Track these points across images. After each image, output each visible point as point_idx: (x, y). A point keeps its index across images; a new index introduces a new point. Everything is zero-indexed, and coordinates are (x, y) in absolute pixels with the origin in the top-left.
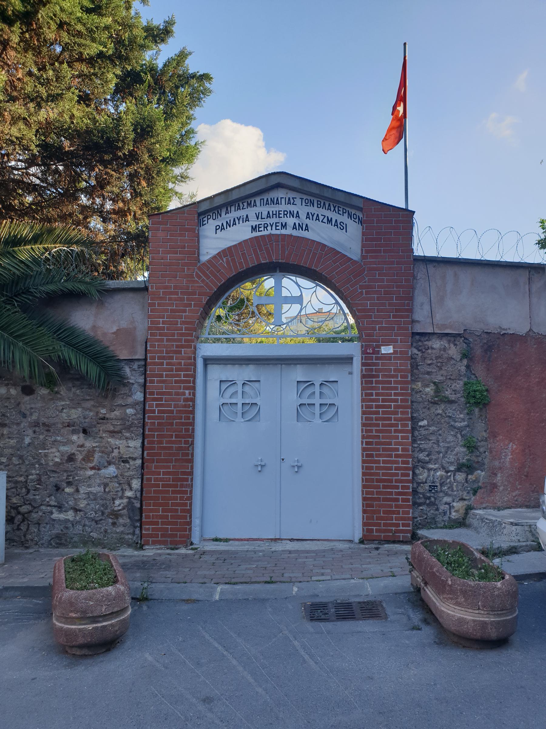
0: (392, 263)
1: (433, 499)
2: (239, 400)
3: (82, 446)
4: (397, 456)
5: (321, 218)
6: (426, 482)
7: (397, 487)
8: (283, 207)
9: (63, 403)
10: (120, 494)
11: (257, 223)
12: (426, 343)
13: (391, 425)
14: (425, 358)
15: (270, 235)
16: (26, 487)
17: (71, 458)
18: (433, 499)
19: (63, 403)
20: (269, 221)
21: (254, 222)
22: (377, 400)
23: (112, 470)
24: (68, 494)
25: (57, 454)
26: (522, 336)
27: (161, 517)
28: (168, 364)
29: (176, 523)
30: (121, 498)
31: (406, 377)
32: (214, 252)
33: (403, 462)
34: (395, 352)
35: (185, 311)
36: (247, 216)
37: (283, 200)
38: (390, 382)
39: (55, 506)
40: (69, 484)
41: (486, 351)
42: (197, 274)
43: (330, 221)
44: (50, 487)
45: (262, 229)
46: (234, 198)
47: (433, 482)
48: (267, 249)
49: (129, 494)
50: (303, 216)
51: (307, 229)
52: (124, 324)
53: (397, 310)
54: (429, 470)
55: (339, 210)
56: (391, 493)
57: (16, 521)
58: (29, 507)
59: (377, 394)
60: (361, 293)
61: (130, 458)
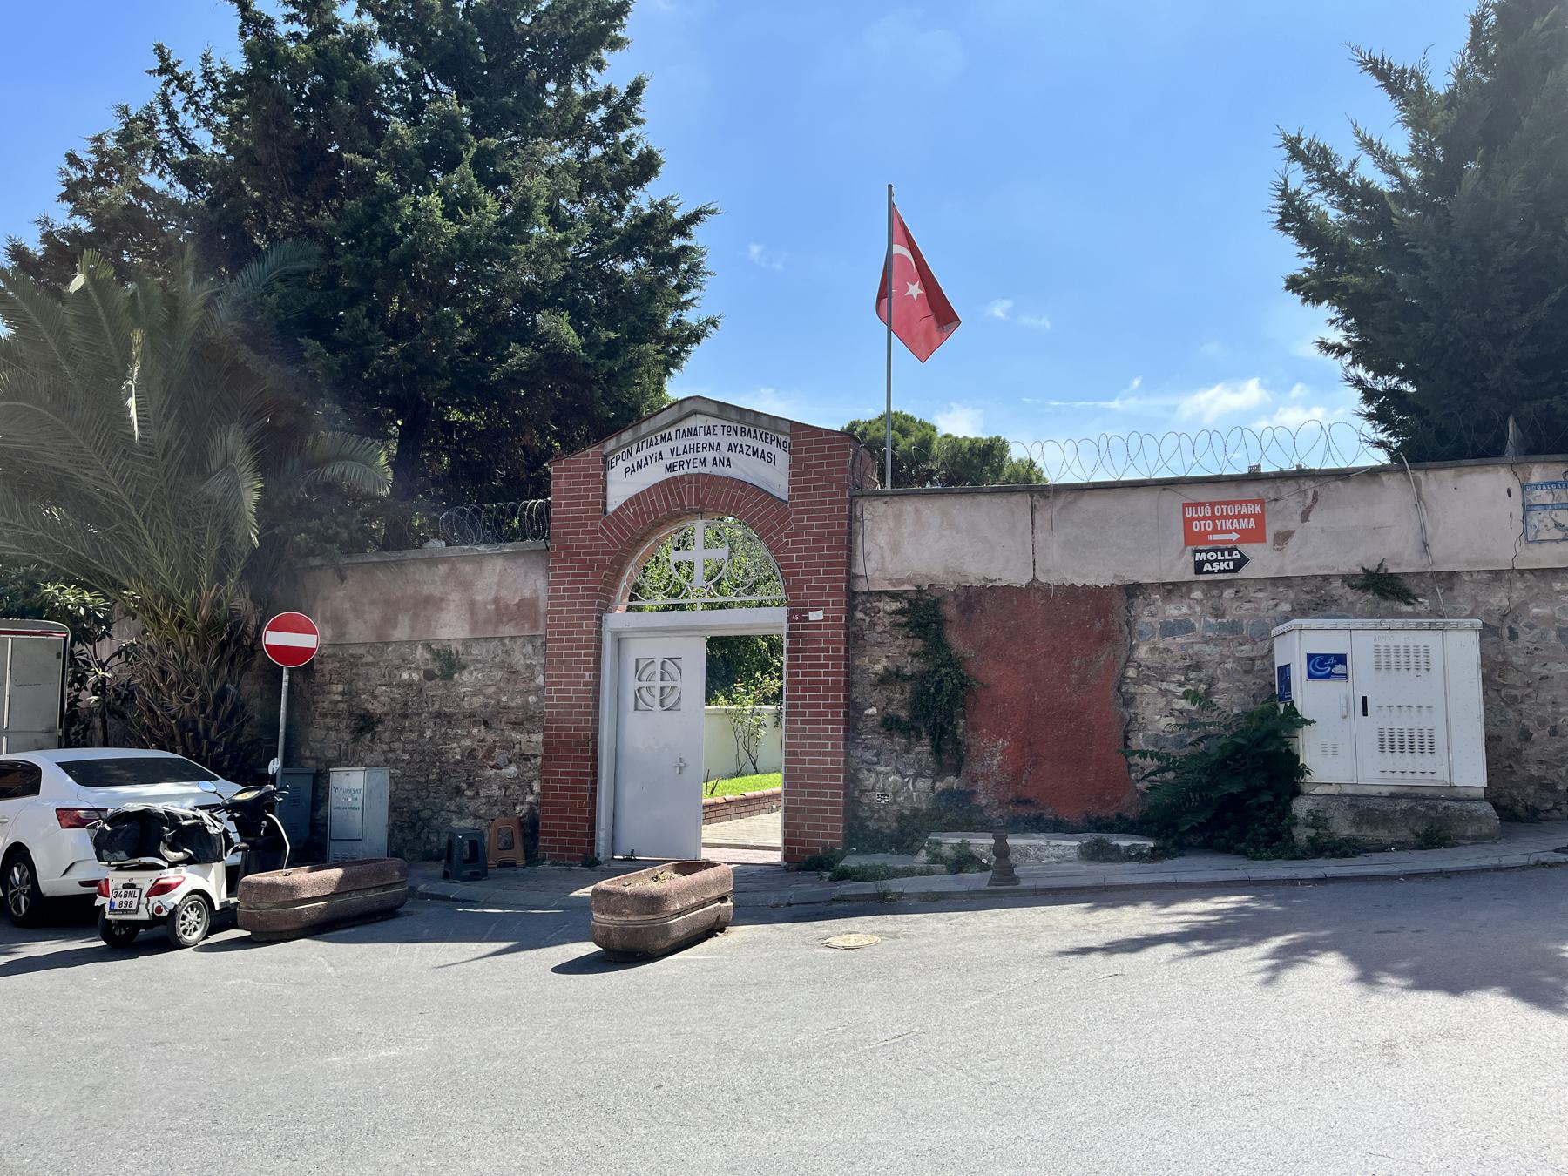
0: (823, 503)
1: (882, 813)
2: (658, 684)
3: (483, 740)
4: (826, 754)
5: (745, 449)
6: (873, 790)
7: (825, 795)
8: (702, 438)
9: (465, 690)
10: (521, 798)
11: (672, 461)
12: (877, 604)
13: (820, 714)
14: (875, 624)
15: (687, 475)
16: (426, 789)
17: (471, 754)
18: (882, 813)
19: (465, 690)
20: (685, 457)
21: (668, 460)
22: (803, 682)
23: (512, 769)
24: (469, 798)
25: (458, 750)
26: (1021, 588)
27: (559, 826)
28: (568, 640)
29: (573, 835)
30: (522, 803)
31: (839, 650)
32: (621, 501)
33: (833, 762)
34: (826, 619)
35: (586, 575)
36: (661, 454)
37: (702, 429)
38: (819, 658)
39: (455, 812)
40: (470, 785)
41: (963, 612)
42: (601, 529)
43: (755, 452)
44: (450, 789)
45: (677, 468)
46: (643, 433)
47: (883, 791)
48: (679, 494)
49: (530, 798)
50: (724, 448)
51: (729, 465)
52: (527, 593)
53: (829, 564)
54: (878, 774)
55: (766, 438)
56: (817, 802)
57: (417, 827)
58: (429, 812)
59: (804, 674)
60: (787, 543)
61: (532, 755)
